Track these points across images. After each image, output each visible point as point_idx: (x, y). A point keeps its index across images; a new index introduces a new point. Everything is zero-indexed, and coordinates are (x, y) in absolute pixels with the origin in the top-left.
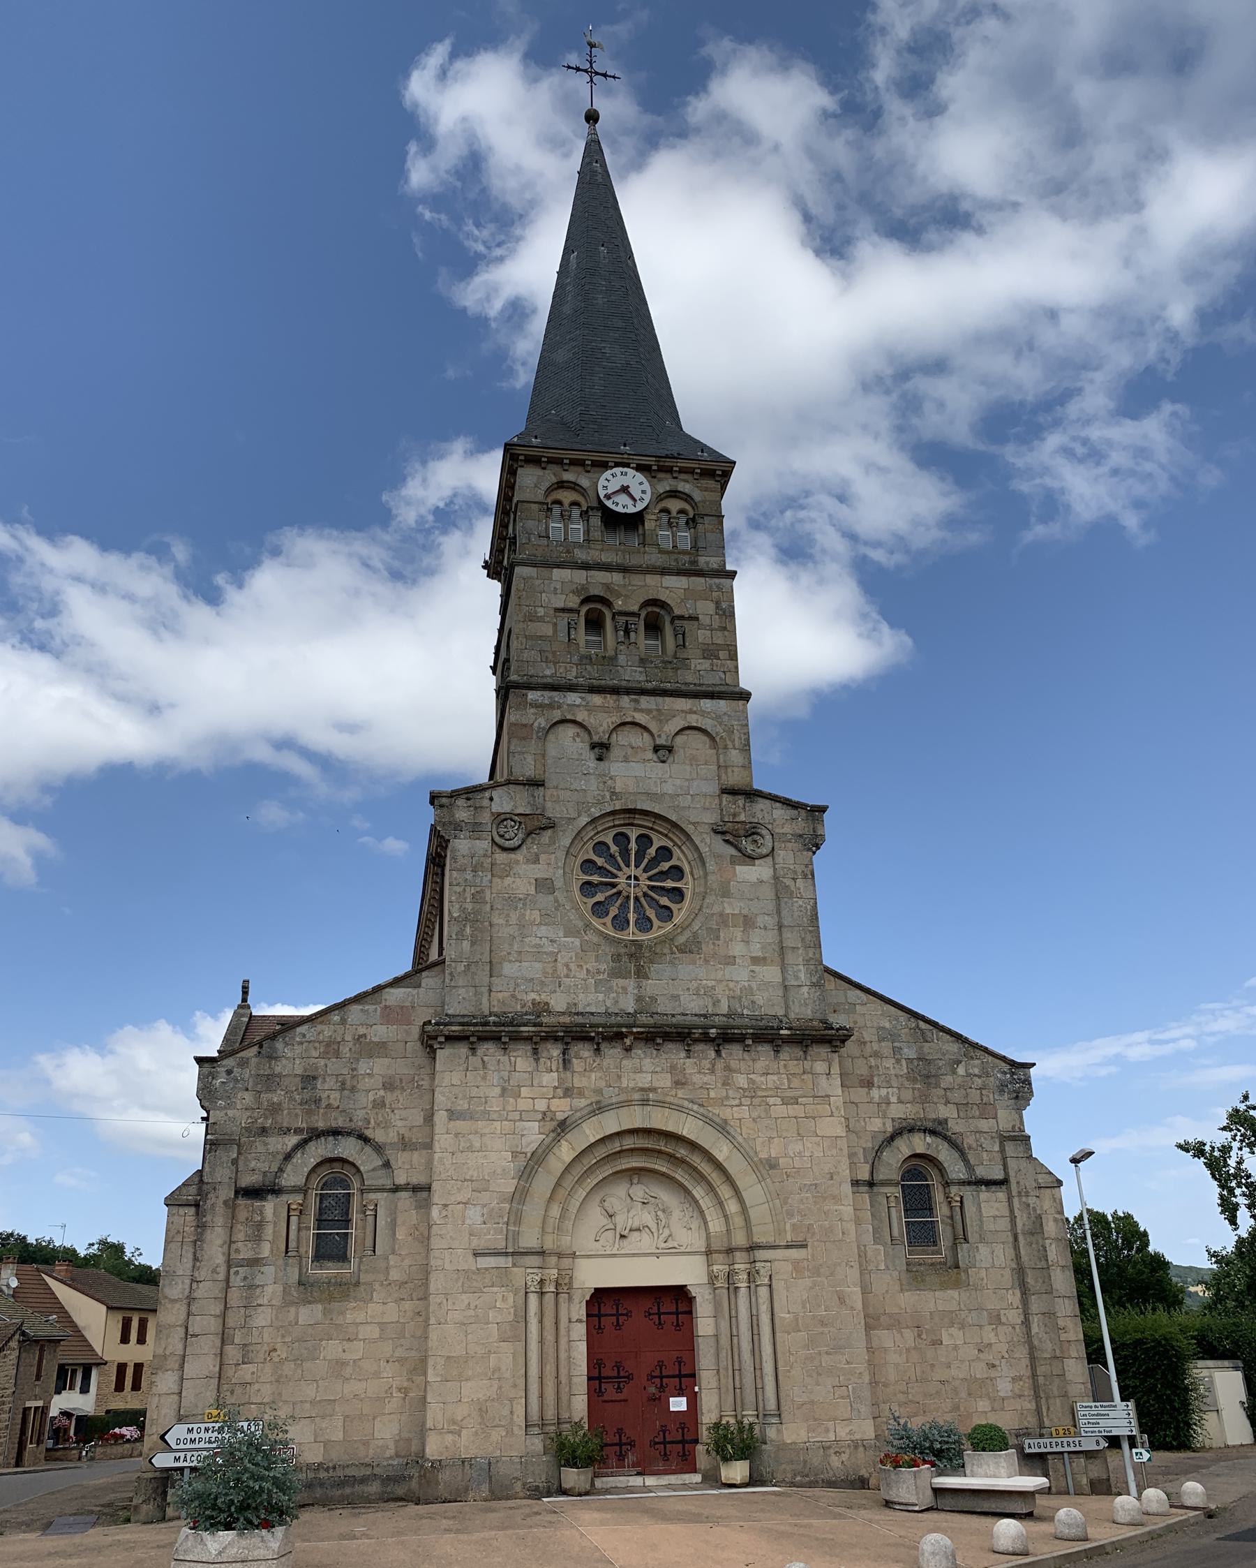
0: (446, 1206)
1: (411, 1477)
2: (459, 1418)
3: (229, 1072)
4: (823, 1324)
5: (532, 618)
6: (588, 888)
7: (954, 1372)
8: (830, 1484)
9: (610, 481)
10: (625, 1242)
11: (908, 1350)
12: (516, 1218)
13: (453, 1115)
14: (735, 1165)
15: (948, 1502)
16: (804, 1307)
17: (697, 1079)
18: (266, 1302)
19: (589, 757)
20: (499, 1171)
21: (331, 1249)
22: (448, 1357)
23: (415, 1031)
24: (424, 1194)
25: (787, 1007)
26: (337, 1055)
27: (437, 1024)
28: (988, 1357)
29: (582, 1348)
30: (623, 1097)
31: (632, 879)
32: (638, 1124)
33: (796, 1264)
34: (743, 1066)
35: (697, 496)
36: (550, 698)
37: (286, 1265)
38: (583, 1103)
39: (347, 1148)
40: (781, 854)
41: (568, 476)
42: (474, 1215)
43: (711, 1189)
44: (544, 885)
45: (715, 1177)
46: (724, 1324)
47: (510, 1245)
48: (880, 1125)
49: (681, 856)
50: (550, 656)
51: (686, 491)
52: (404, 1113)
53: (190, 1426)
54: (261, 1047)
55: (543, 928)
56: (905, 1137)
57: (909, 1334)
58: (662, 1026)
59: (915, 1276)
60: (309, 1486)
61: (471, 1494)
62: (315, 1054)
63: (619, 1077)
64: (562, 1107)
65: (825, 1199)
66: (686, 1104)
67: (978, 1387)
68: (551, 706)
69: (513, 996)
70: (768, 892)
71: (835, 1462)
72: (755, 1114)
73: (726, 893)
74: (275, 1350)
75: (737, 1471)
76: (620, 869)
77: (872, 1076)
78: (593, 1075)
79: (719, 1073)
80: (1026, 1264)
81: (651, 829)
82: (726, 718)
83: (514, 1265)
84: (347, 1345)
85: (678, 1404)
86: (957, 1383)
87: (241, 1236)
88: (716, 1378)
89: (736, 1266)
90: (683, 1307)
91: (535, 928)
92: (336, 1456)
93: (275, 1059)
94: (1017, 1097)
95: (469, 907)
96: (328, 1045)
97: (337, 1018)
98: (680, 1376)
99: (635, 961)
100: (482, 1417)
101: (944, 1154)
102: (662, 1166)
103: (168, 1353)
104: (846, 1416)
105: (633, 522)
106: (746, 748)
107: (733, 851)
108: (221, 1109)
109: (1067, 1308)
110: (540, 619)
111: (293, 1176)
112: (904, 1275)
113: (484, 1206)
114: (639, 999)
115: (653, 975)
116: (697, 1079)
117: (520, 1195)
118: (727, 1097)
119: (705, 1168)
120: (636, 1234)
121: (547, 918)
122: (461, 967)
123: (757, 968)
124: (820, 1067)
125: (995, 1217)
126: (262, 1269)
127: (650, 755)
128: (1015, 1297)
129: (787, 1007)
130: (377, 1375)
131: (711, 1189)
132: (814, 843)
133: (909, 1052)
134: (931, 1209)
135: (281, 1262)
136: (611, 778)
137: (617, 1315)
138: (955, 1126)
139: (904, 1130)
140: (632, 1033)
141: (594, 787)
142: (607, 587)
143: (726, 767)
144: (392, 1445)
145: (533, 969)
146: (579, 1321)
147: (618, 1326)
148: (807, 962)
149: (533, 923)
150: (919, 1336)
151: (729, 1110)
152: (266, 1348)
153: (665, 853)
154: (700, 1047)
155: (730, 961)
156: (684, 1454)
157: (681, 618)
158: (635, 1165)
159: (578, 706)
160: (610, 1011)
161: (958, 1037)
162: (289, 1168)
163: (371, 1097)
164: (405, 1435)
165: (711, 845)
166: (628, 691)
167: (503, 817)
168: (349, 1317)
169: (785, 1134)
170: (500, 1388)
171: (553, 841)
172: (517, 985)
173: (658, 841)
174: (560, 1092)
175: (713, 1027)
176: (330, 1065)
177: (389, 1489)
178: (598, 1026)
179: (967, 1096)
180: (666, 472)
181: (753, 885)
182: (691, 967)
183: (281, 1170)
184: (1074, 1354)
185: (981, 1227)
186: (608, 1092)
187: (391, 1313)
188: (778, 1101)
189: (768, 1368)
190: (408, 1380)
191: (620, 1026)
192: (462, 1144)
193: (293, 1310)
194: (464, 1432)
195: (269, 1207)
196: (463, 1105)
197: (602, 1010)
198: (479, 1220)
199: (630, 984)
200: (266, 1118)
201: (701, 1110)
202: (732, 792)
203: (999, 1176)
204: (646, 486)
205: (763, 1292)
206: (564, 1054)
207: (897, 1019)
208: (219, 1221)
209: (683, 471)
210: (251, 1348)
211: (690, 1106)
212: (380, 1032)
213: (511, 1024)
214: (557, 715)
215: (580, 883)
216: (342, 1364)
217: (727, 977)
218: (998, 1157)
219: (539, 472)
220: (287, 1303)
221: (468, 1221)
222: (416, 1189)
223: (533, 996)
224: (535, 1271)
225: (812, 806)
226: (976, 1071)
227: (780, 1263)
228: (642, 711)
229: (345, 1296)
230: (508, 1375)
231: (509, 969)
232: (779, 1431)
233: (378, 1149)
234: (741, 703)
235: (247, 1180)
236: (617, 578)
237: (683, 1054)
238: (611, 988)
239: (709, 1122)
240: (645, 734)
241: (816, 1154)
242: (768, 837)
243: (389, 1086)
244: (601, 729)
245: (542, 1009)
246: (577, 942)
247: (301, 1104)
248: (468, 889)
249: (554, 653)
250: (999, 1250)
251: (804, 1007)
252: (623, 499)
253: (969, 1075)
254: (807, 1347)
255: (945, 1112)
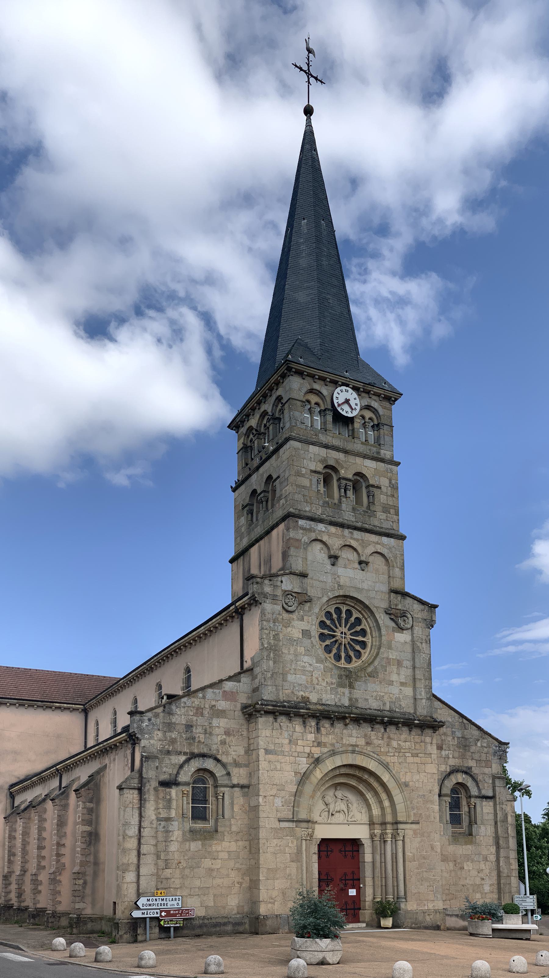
0: (265, 796)
1: (245, 923)
2: (274, 897)
3: (150, 720)
4: (424, 858)
5: (299, 474)
6: (322, 637)
7: (468, 881)
8: (426, 928)
9: (342, 394)
10: (333, 817)
11: (451, 871)
12: (295, 804)
13: (267, 752)
14: (391, 785)
15: (497, 934)
16: (417, 851)
17: (377, 742)
18: (175, 839)
19: (328, 562)
20: (289, 781)
21: (199, 814)
22: (268, 869)
23: (239, 707)
24: (246, 790)
25: (415, 709)
26: (202, 715)
27: (262, 704)
28: (481, 875)
29: (316, 866)
30: (344, 749)
31: (343, 633)
32: (350, 762)
33: (415, 831)
34: (395, 737)
35: (381, 411)
36: (310, 525)
37: (183, 821)
38: (325, 750)
39: (209, 764)
40: (416, 629)
41: (316, 386)
42: (278, 802)
43: (376, 794)
44: (306, 633)
45: (379, 789)
46: (378, 857)
47: (295, 817)
48: (444, 768)
49: (366, 624)
50: (308, 499)
51: (376, 407)
52: (235, 748)
53: (148, 898)
54: (164, 707)
55: (306, 657)
56: (454, 774)
57: (451, 864)
58: (364, 715)
59: (455, 838)
60: (201, 926)
61: (281, 931)
62: (191, 713)
63: (342, 738)
64: (317, 752)
65: (427, 802)
66: (371, 754)
67: (478, 888)
68: (310, 530)
69: (293, 692)
70: (409, 649)
71: (428, 918)
72: (400, 761)
73: (390, 647)
74: (180, 863)
75: (388, 922)
76: (337, 628)
77: (442, 745)
78: (330, 736)
79: (385, 739)
80: (500, 835)
81: (353, 607)
82: (394, 549)
83: (296, 827)
84: (213, 861)
85: (352, 892)
86: (469, 886)
87: (161, 806)
88: (372, 881)
89: (387, 831)
90: (355, 849)
91: (302, 656)
92: (211, 913)
93: (172, 714)
94: (500, 759)
95: (272, 642)
96: (197, 709)
97: (201, 695)
98: (353, 880)
99: (348, 679)
100: (284, 896)
101: (470, 783)
102: (353, 782)
103: (130, 862)
104: (432, 899)
105: (348, 421)
106: (402, 568)
107: (393, 625)
108: (147, 739)
109: (513, 855)
110: (303, 476)
111: (185, 776)
112: (450, 838)
113: (283, 798)
114: (350, 699)
115: (356, 687)
116: (377, 742)
117: (297, 794)
118: (389, 752)
119: (375, 784)
120: (338, 814)
121: (308, 652)
122: (269, 675)
123: (403, 688)
124: (428, 739)
125: (488, 813)
126: (173, 823)
127: (357, 565)
128: (493, 850)
129: (415, 709)
130: (228, 876)
131: (376, 794)
132: (430, 624)
133: (459, 734)
134: (459, 808)
135: (180, 820)
136: (338, 576)
137: (327, 851)
138: (475, 771)
139: (454, 771)
140: (350, 717)
141: (330, 581)
142: (337, 461)
143: (393, 577)
144: (236, 909)
145: (302, 679)
146: (315, 853)
147: (327, 856)
148: (425, 687)
149: (301, 654)
150: (455, 865)
151: (389, 758)
152: (176, 861)
153: (358, 621)
154: (377, 726)
155: (391, 683)
156: (354, 915)
157: (373, 486)
158: (342, 781)
159: (324, 532)
160: (337, 704)
161: (479, 728)
162: (182, 772)
163: (219, 738)
164: (241, 904)
165: (383, 619)
166: (349, 527)
167: (287, 593)
168: (214, 848)
169: (412, 771)
170: (291, 883)
171: (310, 610)
172: (294, 687)
173: (355, 615)
174: (315, 744)
175: (386, 717)
176: (199, 720)
177: (236, 929)
178: (335, 712)
179: (480, 757)
180: (366, 393)
181: (402, 644)
182: (373, 685)
183: (178, 773)
184: (514, 875)
185: (482, 817)
186: (337, 745)
187: (233, 847)
188: (410, 755)
189: (401, 877)
190: (242, 878)
191: (346, 713)
192: (272, 767)
193: (188, 843)
194: (276, 903)
195: (174, 791)
196: (271, 747)
197: (333, 703)
198: (280, 804)
199: (347, 691)
200: (169, 746)
201: (378, 757)
202: (396, 592)
203: (490, 794)
204: (358, 401)
205: (400, 843)
206: (317, 725)
207: (454, 718)
208: (152, 798)
209: (375, 394)
210: (169, 861)
211: (373, 755)
212: (222, 705)
213: (296, 708)
214: (313, 536)
215: (319, 633)
216: (212, 870)
217: (389, 691)
218: (491, 785)
219: (301, 381)
220: (185, 840)
221: (275, 805)
222: (242, 787)
223: (302, 693)
224: (305, 830)
225: (432, 605)
226: (485, 745)
227: (408, 830)
228: (354, 539)
229: (212, 838)
230: (294, 878)
231: (290, 678)
232: (406, 905)
233: (224, 766)
234: (401, 541)
235: (163, 777)
236: (341, 456)
237: (370, 729)
238: (337, 692)
239: (381, 763)
240: (355, 553)
241: (425, 781)
242: (411, 619)
243: (228, 733)
244: (335, 547)
245: (306, 700)
246: (322, 666)
247: (186, 739)
248: (271, 632)
249: (310, 497)
250: (489, 827)
251: (423, 710)
252: (346, 407)
253: (482, 746)
254: (417, 868)
255: (471, 763)
